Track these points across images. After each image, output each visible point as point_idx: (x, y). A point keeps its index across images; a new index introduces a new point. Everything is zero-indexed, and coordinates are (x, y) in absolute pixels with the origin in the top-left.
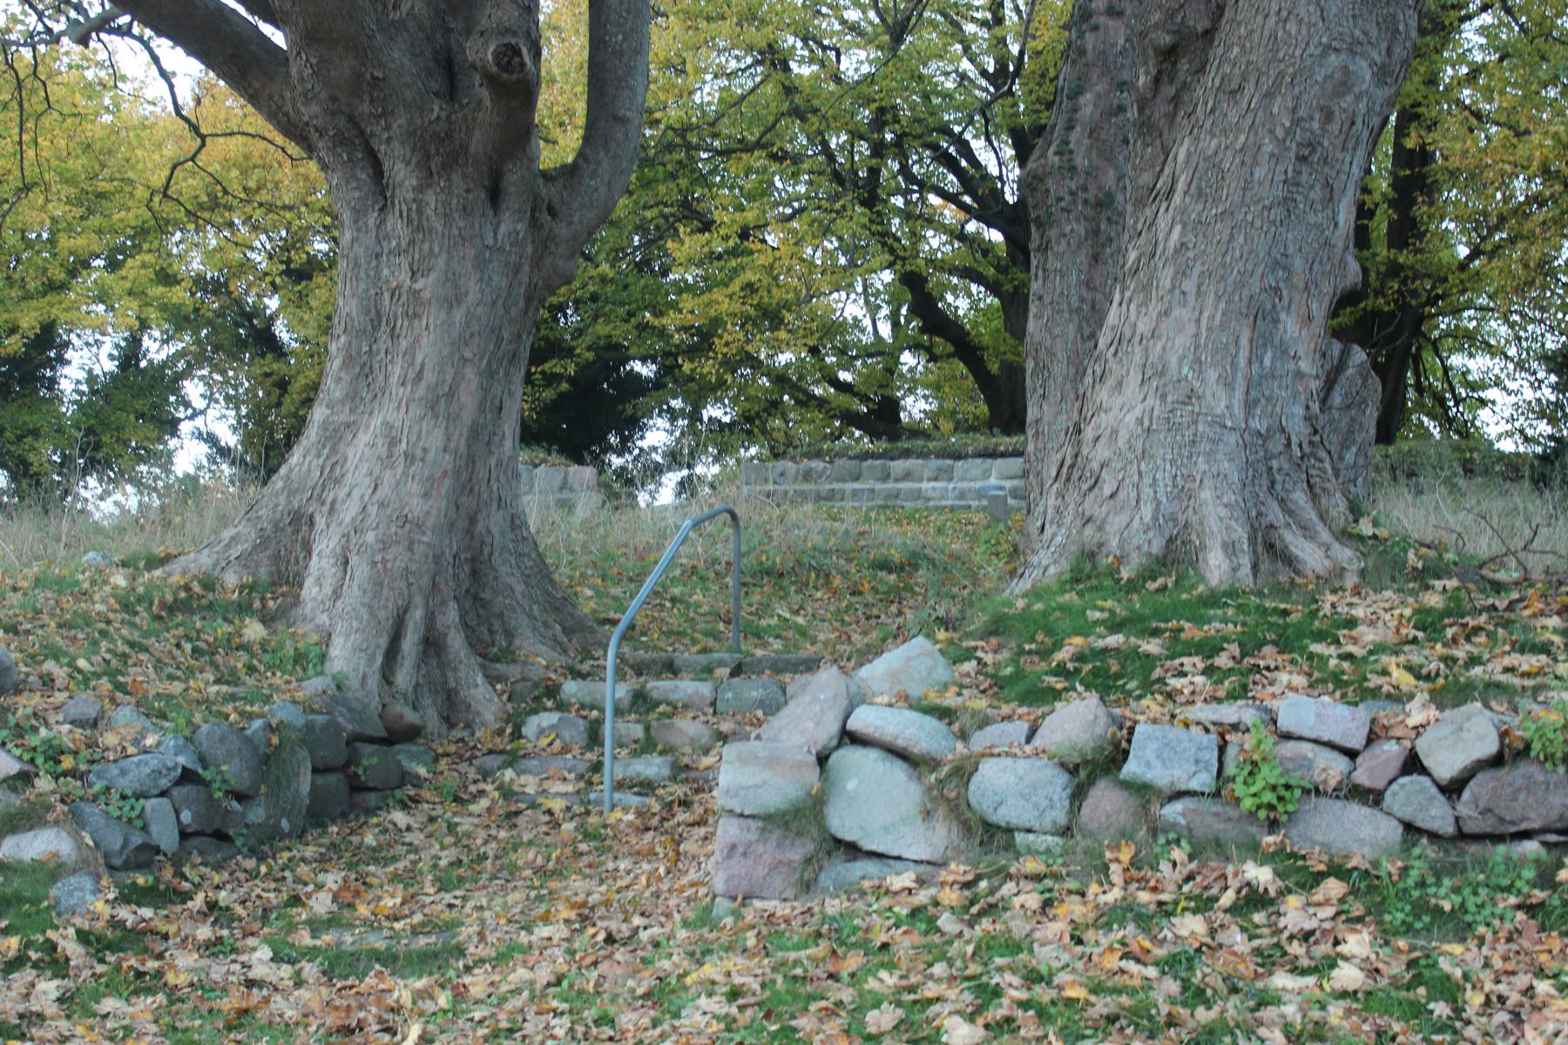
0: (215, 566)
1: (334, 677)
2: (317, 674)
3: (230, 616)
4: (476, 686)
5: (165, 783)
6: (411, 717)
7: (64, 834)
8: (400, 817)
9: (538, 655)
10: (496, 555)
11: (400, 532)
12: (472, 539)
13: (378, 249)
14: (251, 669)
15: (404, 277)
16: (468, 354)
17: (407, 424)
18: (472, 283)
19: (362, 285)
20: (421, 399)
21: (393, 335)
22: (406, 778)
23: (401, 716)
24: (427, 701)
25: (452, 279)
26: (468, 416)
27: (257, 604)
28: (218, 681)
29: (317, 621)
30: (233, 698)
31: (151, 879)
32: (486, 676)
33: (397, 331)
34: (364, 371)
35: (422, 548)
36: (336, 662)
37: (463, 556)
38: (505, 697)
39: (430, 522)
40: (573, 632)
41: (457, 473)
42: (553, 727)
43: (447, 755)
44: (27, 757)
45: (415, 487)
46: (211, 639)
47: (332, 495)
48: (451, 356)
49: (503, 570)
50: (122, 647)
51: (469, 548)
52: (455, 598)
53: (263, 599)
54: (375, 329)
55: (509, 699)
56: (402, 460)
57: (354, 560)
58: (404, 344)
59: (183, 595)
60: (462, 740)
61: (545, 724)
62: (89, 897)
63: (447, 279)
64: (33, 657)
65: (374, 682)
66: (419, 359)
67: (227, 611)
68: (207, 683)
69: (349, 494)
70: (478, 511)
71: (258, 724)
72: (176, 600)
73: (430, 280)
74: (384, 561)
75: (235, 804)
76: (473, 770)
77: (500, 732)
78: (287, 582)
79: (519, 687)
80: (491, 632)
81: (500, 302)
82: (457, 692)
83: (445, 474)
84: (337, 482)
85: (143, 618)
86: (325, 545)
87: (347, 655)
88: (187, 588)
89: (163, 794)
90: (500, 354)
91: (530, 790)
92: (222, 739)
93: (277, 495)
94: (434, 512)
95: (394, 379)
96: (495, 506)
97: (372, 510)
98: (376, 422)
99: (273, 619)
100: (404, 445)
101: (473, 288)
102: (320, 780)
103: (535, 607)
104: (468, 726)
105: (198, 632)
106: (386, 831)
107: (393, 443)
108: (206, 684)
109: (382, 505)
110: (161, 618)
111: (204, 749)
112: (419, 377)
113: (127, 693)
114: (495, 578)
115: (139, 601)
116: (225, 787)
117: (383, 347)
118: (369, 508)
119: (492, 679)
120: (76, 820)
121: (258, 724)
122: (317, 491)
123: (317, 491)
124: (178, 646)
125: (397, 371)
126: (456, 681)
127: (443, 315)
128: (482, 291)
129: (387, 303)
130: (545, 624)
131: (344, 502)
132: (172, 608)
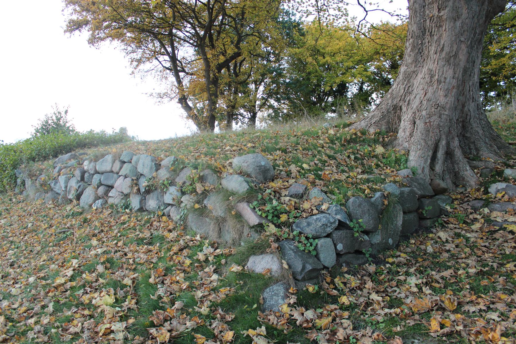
0: (367, 126)
1: (411, 169)
2: (405, 168)
3: (371, 144)
4: (467, 170)
5: (329, 230)
6: (443, 185)
7: (275, 259)
8: (443, 235)
9: (490, 159)
10: (472, 120)
11: (436, 110)
12: (463, 113)
13: (424, 4)
14: (378, 166)
15: (435, 12)
16: (462, 39)
17: (438, 68)
18: (464, 11)
19: (418, 19)
20: (443, 58)
21: (431, 35)
22: (442, 212)
23: (439, 185)
24: (447, 177)
25: (456, 10)
26: (462, 64)
27: (381, 140)
28: (363, 172)
29: (404, 146)
30: (368, 181)
31: (316, 288)
32: (470, 166)
33: (433, 33)
34: (419, 52)
35: (445, 116)
36: (412, 162)
37: (460, 120)
38: (479, 175)
39: (448, 106)
40: (501, 148)
41: (458, 87)
42: (503, 189)
43: (457, 199)
44: (264, 215)
45: (441, 93)
46: (362, 153)
47: (408, 98)
48: (456, 40)
49: (474, 125)
50: (325, 158)
51: (462, 117)
52: (457, 136)
53: (383, 138)
54: (424, 35)
55: (480, 176)
56: (436, 82)
57: (418, 122)
58: (435, 38)
59: (354, 136)
60: (462, 193)
61: (499, 188)
62: (280, 301)
63: (453, 10)
64: (287, 162)
65: (427, 170)
66: (442, 43)
67: (370, 142)
68: (358, 173)
69: (415, 97)
70: (465, 102)
71: (378, 194)
72: (351, 138)
73: (446, 11)
74: (430, 122)
75: (366, 237)
76: (469, 207)
77: (478, 190)
78: (392, 131)
79: (484, 171)
80: (470, 149)
81: (476, 17)
82: (459, 173)
83: (454, 87)
84: (410, 93)
85: (337, 146)
86: (405, 124)
87: (416, 159)
88: (355, 134)
89: (328, 236)
90: (475, 39)
91: (499, 220)
92: (360, 206)
93: (388, 100)
94: (449, 102)
95: (432, 52)
96: (471, 101)
97: (425, 103)
98: (425, 70)
99: (387, 145)
100: (437, 77)
101: (464, 12)
102: (407, 217)
103: (487, 139)
104: (464, 186)
105: (358, 150)
106: (436, 242)
107: (432, 77)
108: (357, 174)
109: (428, 100)
110: (345, 145)
111: (351, 210)
112: (442, 50)
113: (320, 179)
114: (472, 128)
115: (337, 139)
116: (360, 230)
117: (427, 41)
118: (423, 102)
119: (473, 168)
120: (281, 251)
121: (378, 194)
122: (403, 97)
123: (403, 97)
124: (349, 157)
125: (433, 49)
126: (458, 168)
127: (452, 24)
128: (468, 13)
129: (428, 24)
130: (491, 145)
131: (413, 101)
132: (349, 142)
